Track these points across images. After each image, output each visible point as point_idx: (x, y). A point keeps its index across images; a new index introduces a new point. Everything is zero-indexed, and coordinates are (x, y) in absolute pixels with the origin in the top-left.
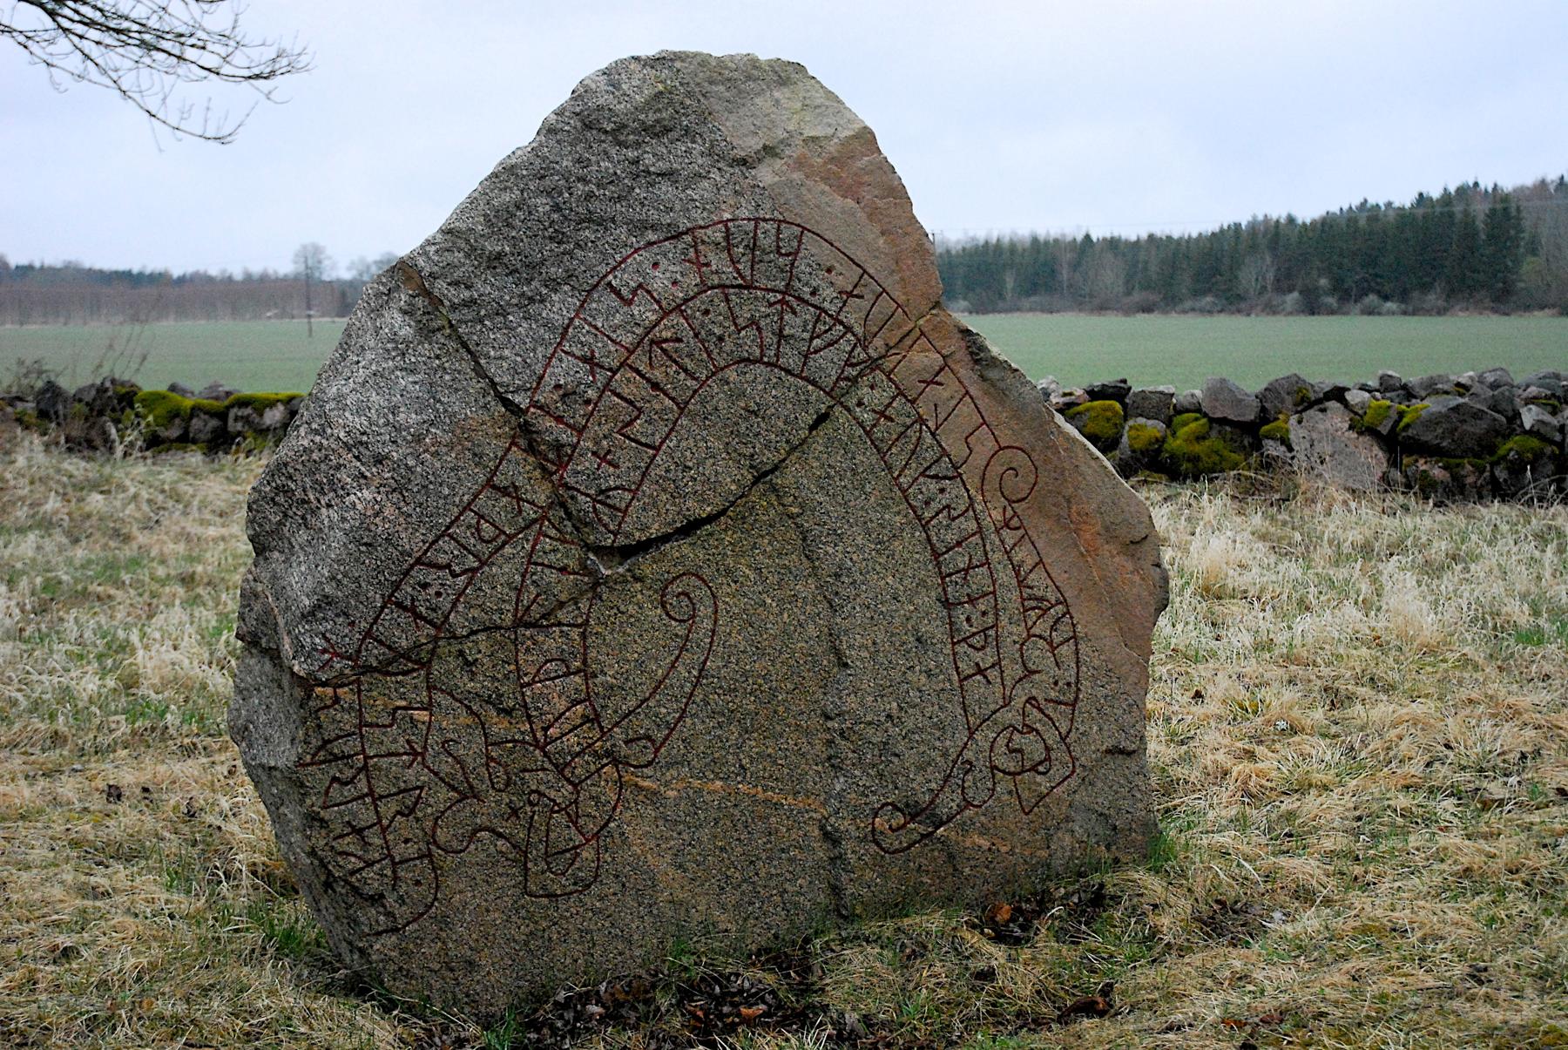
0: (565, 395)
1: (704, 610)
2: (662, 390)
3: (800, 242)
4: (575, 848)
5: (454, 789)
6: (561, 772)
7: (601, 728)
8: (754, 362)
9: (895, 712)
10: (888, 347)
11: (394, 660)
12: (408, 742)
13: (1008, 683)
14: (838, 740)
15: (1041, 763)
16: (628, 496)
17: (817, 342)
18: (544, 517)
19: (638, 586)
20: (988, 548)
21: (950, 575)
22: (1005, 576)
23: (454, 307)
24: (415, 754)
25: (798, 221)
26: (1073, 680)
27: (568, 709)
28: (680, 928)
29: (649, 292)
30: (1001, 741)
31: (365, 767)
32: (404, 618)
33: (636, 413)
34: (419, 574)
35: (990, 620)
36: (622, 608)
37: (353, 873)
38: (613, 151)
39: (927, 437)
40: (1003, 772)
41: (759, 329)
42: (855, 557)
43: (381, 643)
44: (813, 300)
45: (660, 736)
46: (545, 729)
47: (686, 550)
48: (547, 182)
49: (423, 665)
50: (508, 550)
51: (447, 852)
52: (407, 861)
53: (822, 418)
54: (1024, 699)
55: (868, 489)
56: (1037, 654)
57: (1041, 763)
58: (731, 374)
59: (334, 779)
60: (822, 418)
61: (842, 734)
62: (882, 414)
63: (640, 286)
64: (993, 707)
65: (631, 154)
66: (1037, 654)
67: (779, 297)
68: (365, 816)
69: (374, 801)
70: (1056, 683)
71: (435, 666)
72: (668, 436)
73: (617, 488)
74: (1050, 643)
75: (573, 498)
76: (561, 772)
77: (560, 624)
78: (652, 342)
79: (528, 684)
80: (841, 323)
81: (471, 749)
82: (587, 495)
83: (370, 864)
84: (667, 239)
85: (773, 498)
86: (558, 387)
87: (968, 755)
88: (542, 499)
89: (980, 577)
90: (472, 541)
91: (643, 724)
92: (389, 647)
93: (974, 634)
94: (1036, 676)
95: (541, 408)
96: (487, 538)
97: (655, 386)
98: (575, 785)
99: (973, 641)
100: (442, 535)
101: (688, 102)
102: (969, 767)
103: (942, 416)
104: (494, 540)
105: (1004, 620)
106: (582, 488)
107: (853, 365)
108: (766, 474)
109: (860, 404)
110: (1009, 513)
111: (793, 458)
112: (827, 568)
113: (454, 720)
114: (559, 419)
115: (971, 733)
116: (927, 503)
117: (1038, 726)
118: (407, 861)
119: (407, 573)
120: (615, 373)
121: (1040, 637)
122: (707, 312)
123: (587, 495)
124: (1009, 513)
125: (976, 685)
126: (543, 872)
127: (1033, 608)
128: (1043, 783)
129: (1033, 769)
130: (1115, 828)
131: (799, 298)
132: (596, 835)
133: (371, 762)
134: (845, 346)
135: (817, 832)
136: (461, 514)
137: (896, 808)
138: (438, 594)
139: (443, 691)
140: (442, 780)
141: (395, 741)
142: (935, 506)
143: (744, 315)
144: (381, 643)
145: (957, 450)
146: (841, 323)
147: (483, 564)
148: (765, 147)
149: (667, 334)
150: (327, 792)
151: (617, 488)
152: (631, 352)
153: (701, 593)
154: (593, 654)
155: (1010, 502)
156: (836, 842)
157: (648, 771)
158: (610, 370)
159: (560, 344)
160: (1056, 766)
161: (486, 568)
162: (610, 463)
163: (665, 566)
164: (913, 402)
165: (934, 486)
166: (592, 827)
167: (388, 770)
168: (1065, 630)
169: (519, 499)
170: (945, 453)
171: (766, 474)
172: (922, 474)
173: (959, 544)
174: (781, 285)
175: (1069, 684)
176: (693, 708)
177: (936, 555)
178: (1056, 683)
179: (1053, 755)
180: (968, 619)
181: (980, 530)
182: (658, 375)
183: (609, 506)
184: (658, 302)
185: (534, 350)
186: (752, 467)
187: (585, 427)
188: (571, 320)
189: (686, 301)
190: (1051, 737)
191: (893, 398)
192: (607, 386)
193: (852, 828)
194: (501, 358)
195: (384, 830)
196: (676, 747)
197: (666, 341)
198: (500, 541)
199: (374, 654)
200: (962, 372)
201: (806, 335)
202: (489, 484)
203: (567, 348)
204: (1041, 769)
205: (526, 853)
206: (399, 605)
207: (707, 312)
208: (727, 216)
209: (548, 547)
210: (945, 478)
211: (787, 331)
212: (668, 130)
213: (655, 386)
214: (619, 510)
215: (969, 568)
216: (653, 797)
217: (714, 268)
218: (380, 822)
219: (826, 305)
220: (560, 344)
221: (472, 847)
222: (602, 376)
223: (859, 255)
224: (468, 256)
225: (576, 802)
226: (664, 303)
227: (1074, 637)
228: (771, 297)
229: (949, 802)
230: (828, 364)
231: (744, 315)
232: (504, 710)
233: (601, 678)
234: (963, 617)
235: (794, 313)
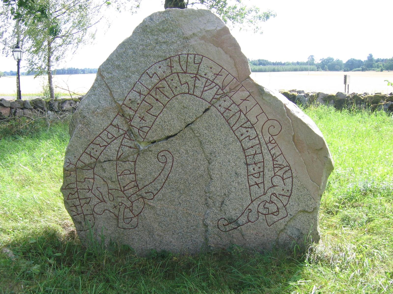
0: (132, 102)
1: (170, 160)
2: (159, 101)
3: (202, 60)
4: (131, 218)
5: (99, 199)
6: (128, 198)
7: (139, 189)
8: (186, 93)
9: (227, 193)
10: (230, 89)
11: (85, 166)
12: (88, 186)
13: (266, 189)
14: (208, 199)
15: (275, 212)
16: (148, 129)
17: (206, 88)
18: (125, 134)
19: (151, 153)
20: (262, 148)
21: (248, 156)
22: (268, 157)
23: (107, 79)
24: (90, 190)
25: (202, 54)
26: (290, 189)
27: (130, 183)
28: (161, 242)
29: (157, 75)
30: (262, 205)
31: (77, 191)
32: (88, 157)
33: (151, 107)
34: (92, 146)
35: (261, 169)
36: (146, 158)
37: (74, 216)
38: (151, 38)
39: (242, 116)
40: (262, 214)
41: (188, 84)
42: (216, 149)
43: (82, 162)
44: (205, 76)
45: (155, 192)
46: (124, 187)
47: (165, 144)
48: (132, 46)
49: (92, 168)
50: (115, 141)
51: (97, 214)
52: (87, 215)
53: (207, 110)
54: (271, 194)
55: (222, 130)
56: (277, 180)
57: (275, 212)
58: (179, 97)
59: (70, 193)
60: (207, 110)
61: (209, 198)
62: (227, 109)
63: (155, 73)
64: (260, 195)
65: (155, 37)
66: (277, 180)
67: (195, 75)
68: (77, 203)
69: (79, 199)
70: (283, 190)
71: (95, 168)
72: (160, 113)
73: (145, 127)
74: (283, 178)
75: (133, 129)
76: (128, 198)
77: (129, 161)
78: (156, 88)
79: (120, 176)
80: (214, 83)
81: (104, 190)
82: (137, 128)
83: (78, 214)
84: (164, 60)
85: (191, 131)
86: (130, 100)
87: (250, 207)
88: (125, 129)
89: (259, 158)
90: (106, 138)
91: (150, 188)
92: (84, 163)
93: (255, 173)
94: (276, 187)
95: (125, 105)
96: (109, 138)
97: (157, 100)
98: (132, 202)
99: (255, 175)
100: (98, 137)
101: (172, 23)
102: (250, 211)
103: (248, 110)
104: (112, 138)
105: (266, 171)
106: (135, 126)
107: (218, 95)
108: (189, 124)
109: (220, 106)
110: (271, 139)
111: (198, 120)
112: (207, 151)
113: (99, 182)
114: (130, 108)
115: (252, 202)
116: (242, 135)
117: (275, 202)
118: (87, 215)
119: (89, 145)
120: (146, 96)
121: (279, 176)
122: (172, 80)
123: (137, 128)
124: (271, 139)
125: (255, 188)
126: (122, 222)
127: (277, 167)
128: (276, 218)
129: (272, 213)
130: (302, 233)
131: (200, 76)
132: (138, 215)
133: (79, 190)
134: (215, 89)
135: (202, 223)
136: (103, 131)
137: (225, 220)
138: (96, 151)
139: (97, 175)
140: (96, 196)
141: (85, 185)
142: (244, 136)
143: (183, 81)
144: (82, 162)
145: (253, 120)
146: (214, 83)
147: (109, 144)
148: (194, 34)
149: (161, 86)
150: (68, 196)
151: (145, 127)
152: (151, 91)
153: (169, 155)
154: (137, 169)
155: (272, 136)
156: (207, 226)
157: (152, 201)
158: (144, 95)
159: (133, 88)
160: (281, 214)
161: (109, 145)
162: (144, 120)
163: (158, 148)
164: (238, 106)
165: (244, 130)
166: (136, 213)
167: (82, 193)
168: (289, 174)
169: (119, 128)
170: (248, 121)
171: (189, 124)
172: (241, 126)
173: (252, 147)
174: (196, 72)
175: (288, 191)
176: (165, 186)
177: (244, 150)
178: (283, 190)
179: (280, 210)
180: (254, 169)
181: (260, 143)
182: (158, 97)
183: (143, 131)
184: (159, 77)
185: (125, 90)
186: (185, 122)
187: (137, 110)
188: (136, 82)
189: (166, 77)
190: (280, 205)
191: (232, 104)
192: (143, 100)
193: (211, 223)
194: (117, 92)
195: (82, 207)
196: (160, 195)
197: (160, 88)
198: (113, 139)
199: (80, 164)
200: (256, 97)
201: (203, 86)
202: (111, 124)
203: (134, 89)
204: (275, 214)
205: (118, 217)
206: (87, 153)
207: (172, 80)
208: (179, 53)
209: (126, 141)
210: (249, 128)
211: (196, 85)
212: (166, 31)
213: (157, 100)
214: (145, 132)
215: (255, 154)
216: (153, 208)
217: (175, 67)
218: (80, 205)
219: (209, 78)
220: (133, 88)
221: (104, 214)
222: (142, 97)
223: (221, 64)
224: (112, 66)
225: (132, 206)
226: (160, 77)
227: (292, 177)
228: (192, 76)
229: (242, 220)
230: (209, 94)
231: (183, 81)
232: (112, 181)
233: (139, 176)
234: (252, 168)
235: (199, 80)
